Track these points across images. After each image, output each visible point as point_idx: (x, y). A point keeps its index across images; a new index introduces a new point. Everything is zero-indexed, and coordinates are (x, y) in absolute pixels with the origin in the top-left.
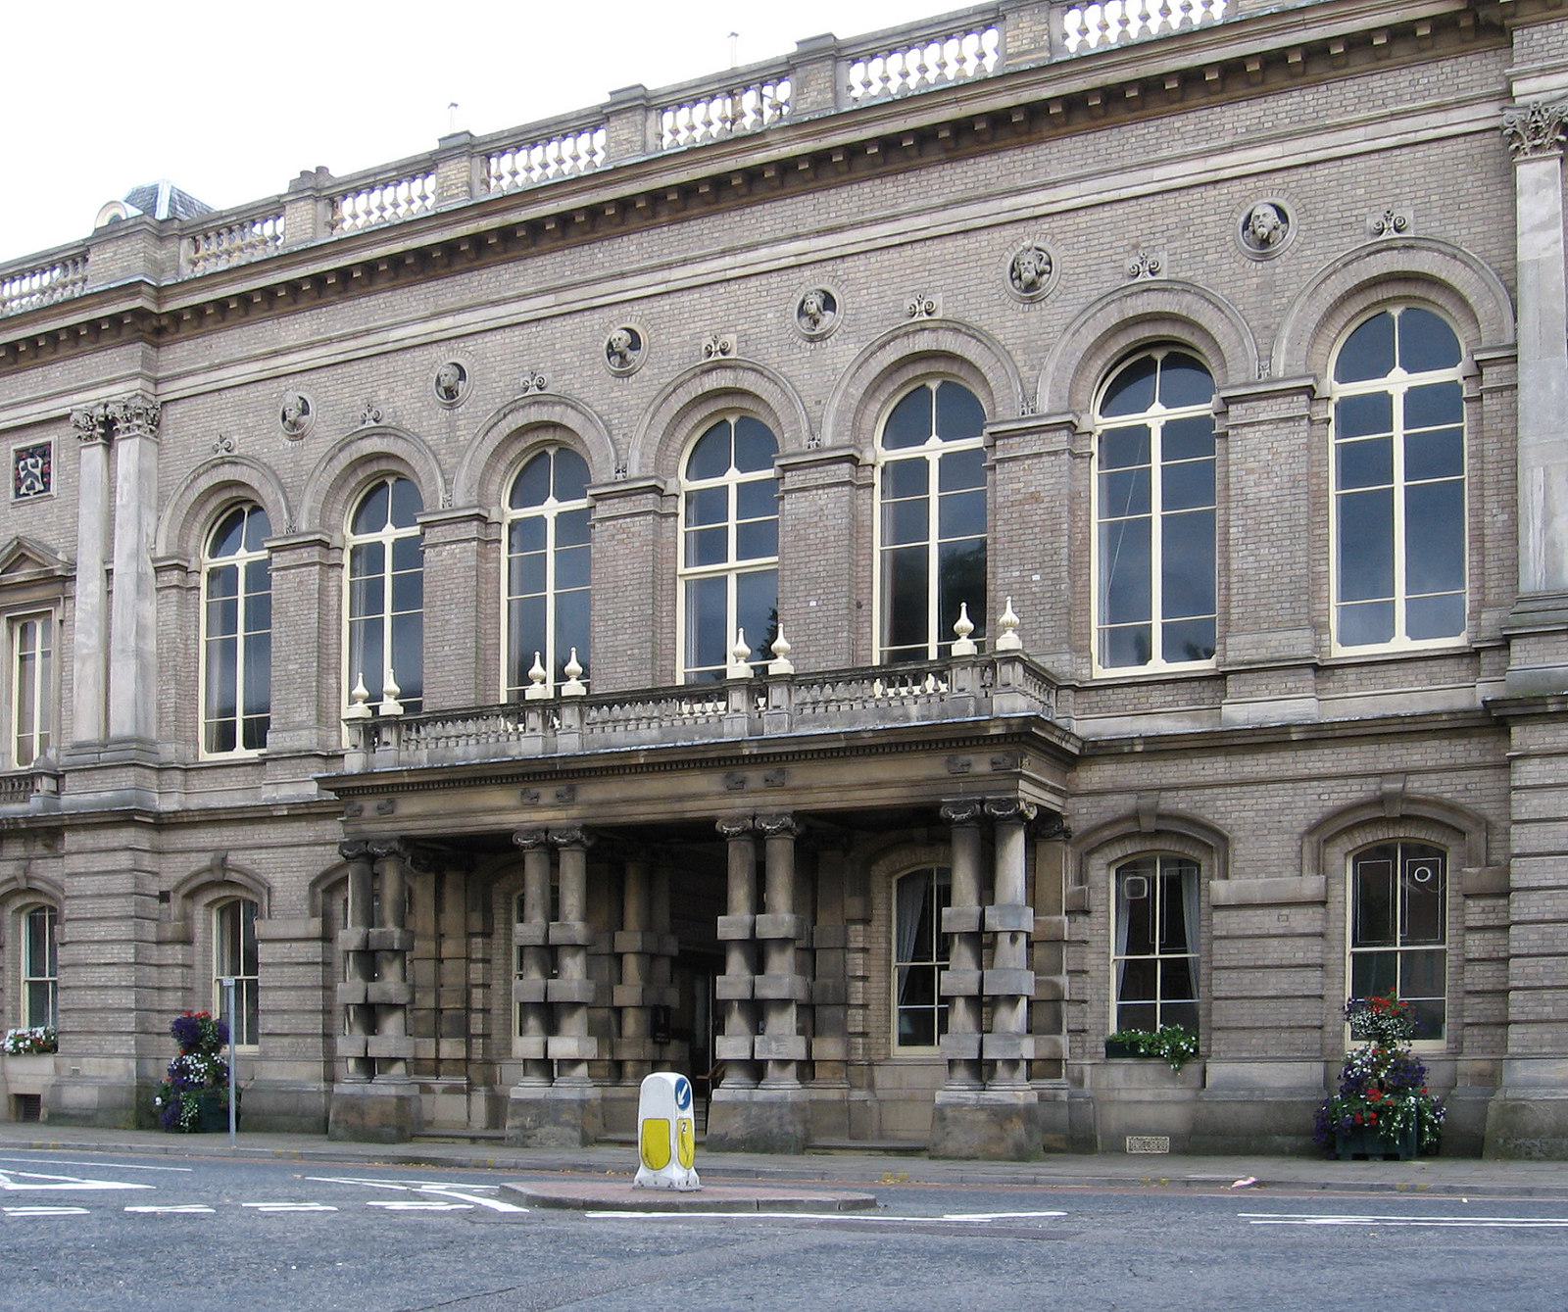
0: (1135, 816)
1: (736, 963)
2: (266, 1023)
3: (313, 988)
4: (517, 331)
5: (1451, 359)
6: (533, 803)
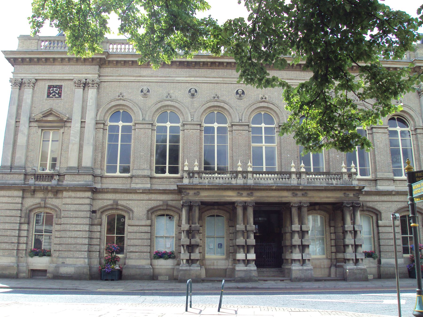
3: (147, 239)
4: (211, 84)
5: (131, 122)
6: (241, 195)
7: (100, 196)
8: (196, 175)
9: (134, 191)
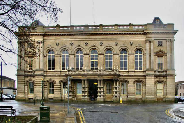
0: (123, 80)
1: (99, 89)
2: (55, 92)
7: (46, 77)
8: (83, 71)
9: (55, 76)
